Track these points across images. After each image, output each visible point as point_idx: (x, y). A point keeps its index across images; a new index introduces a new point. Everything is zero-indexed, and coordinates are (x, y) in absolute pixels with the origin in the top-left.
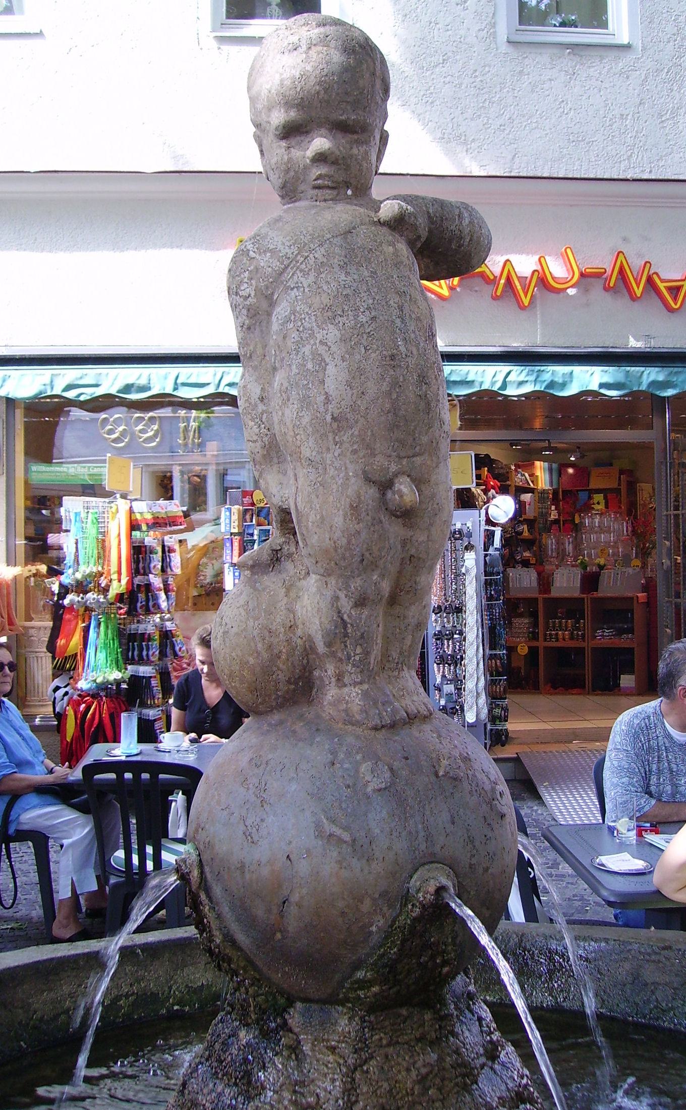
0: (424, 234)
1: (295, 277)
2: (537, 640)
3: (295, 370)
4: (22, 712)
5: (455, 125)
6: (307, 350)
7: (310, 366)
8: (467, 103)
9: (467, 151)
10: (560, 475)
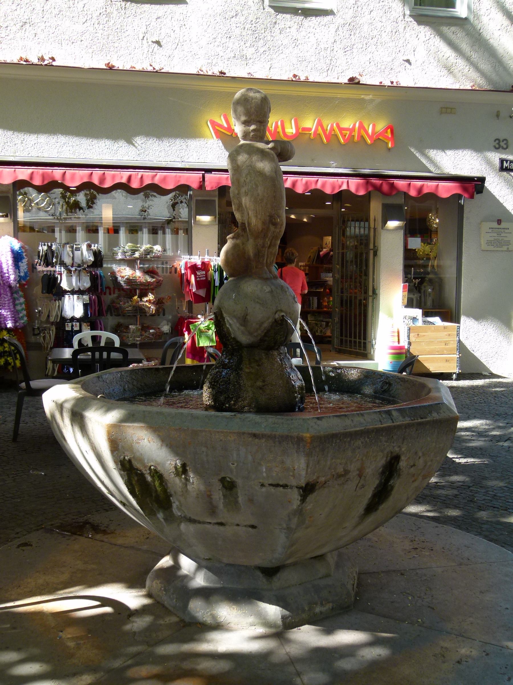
0: (279, 151)
4: (52, 294)
5: (241, 50)
7: (254, 186)
8: (247, 38)
9: (247, 64)
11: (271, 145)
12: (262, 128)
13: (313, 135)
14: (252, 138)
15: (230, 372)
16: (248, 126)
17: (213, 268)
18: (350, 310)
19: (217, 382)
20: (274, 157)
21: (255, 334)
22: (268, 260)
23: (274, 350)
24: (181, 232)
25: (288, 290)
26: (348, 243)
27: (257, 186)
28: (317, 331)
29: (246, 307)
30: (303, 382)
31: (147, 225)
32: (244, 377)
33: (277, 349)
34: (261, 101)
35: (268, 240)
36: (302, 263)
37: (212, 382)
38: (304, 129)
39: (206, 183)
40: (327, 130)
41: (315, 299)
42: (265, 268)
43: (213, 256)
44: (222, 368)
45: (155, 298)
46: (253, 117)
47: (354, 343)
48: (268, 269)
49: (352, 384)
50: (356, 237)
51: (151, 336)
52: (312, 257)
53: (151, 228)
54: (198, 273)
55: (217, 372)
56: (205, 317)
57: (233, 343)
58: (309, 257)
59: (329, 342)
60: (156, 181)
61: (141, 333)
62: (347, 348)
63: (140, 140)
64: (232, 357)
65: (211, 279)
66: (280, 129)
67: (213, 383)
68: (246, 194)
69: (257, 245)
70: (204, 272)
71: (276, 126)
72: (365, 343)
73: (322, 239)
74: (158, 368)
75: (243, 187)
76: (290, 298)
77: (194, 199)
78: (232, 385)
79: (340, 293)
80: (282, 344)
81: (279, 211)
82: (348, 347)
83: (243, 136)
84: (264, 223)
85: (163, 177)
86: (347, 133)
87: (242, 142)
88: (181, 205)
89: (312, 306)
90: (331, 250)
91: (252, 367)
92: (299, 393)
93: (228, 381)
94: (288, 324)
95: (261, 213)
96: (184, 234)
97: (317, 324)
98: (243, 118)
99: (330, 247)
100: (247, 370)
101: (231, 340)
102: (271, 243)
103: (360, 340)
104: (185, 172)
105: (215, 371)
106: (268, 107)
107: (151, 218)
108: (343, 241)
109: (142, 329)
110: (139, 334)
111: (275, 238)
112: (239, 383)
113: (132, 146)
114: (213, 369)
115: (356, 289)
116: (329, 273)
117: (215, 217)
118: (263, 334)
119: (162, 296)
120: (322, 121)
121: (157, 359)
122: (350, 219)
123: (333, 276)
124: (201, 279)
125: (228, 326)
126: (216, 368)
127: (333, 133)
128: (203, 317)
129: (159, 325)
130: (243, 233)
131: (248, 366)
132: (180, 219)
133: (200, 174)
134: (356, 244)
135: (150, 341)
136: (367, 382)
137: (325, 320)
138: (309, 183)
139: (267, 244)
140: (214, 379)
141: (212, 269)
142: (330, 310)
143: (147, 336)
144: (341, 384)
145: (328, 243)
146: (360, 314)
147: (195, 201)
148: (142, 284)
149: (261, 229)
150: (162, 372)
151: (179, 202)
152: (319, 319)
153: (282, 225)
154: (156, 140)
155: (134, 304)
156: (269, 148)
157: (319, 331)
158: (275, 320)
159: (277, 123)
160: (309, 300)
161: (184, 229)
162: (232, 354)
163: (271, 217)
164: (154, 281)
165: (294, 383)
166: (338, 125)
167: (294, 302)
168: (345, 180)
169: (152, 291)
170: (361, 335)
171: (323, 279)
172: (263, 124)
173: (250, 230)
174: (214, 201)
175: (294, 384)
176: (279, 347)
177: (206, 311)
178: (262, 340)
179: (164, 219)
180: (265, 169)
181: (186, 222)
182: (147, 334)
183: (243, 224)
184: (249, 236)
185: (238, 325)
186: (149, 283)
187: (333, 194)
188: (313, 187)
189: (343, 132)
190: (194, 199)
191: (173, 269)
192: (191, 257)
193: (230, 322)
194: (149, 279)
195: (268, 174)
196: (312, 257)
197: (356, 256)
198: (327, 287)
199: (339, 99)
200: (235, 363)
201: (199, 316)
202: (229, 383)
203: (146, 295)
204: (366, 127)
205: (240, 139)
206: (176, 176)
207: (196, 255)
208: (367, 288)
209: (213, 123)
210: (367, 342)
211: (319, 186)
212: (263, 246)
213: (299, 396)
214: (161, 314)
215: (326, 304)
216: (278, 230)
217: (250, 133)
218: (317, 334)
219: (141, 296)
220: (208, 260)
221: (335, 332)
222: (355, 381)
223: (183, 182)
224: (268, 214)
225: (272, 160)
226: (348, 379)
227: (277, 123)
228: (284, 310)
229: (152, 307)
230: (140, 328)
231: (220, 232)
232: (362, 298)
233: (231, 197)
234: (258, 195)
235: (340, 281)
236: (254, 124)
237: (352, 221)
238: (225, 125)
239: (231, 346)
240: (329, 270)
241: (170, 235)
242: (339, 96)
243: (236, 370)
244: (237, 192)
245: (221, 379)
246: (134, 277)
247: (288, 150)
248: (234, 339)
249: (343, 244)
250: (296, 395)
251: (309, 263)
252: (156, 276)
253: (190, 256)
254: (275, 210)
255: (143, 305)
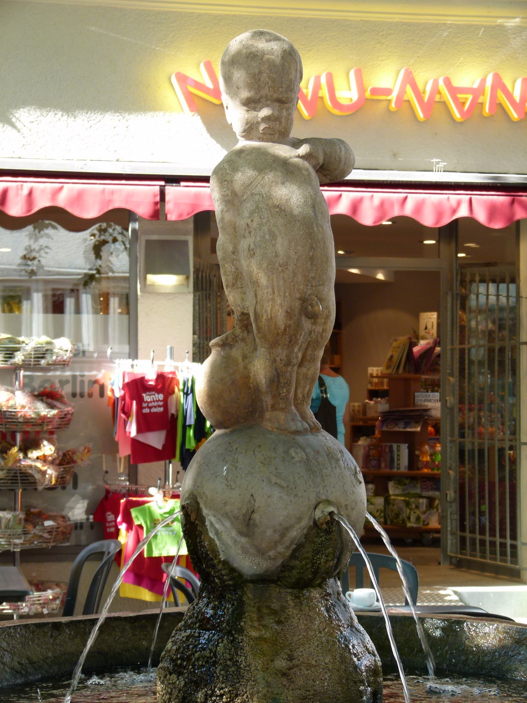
0: (321, 161)
1: (258, 188)
2: (480, 540)
3: (258, 239)
6: (265, 228)
7: (267, 237)
10: (14, 463)
11: (304, 149)
12: (285, 113)
13: (396, 103)
14: (264, 134)
15: (216, 637)
16: (254, 109)
17: (181, 387)
18: (479, 471)
19: (189, 659)
20: (309, 175)
21: (272, 553)
22: (299, 391)
23: (314, 587)
24: (114, 303)
25: (343, 456)
26: (473, 323)
27: (273, 236)
28: (409, 518)
29: (252, 495)
30: (378, 658)
31: (41, 286)
32: (247, 648)
33: (320, 586)
34: (283, 58)
35: (299, 350)
36: (375, 369)
37: (177, 659)
38: (374, 91)
39: (169, 206)
40: (424, 92)
41: (404, 450)
42: (293, 408)
43: (183, 360)
44: (200, 627)
45: (57, 450)
46: (265, 91)
47: (490, 546)
48: (298, 411)
49: (486, 659)
50: (489, 310)
51: (46, 535)
52: (395, 359)
53: (50, 293)
54: (147, 397)
55: (188, 637)
56: (164, 492)
57: (223, 572)
58: (388, 356)
59: (436, 543)
60: (61, 201)
61: (24, 527)
62: (475, 556)
63: (26, 114)
64: (220, 603)
65: (177, 411)
66: (324, 92)
67: (179, 662)
68: (251, 253)
69: (275, 361)
70: (161, 397)
71: (317, 87)
72: (514, 547)
73: (417, 318)
74: (60, 623)
75: (244, 237)
76: (347, 473)
77: (143, 239)
78: (220, 667)
79: (456, 437)
80: (329, 574)
81: (321, 288)
82: (478, 554)
83: (244, 131)
84: (289, 314)
85: (75, 193)
86: (466, 99)
87: (242, 143)
88: (113, 246)
89: (398, 464)
90: (437, 343)
91: (264, 626)
92: (368, 682)
93: (211, 658)
94: (344, 531)
95: (282, 294)
96: (119, 311)
97: (408, 504)
98: (245, 94)
99: (435, 335)
100: (254, 634)
101: (220, 567)
102: (304, 357)
103: (503, 540)
104: (123, 182)
105: (184, 634)
106: (296, 70)
107: (49, 271)
108: (462, 320)
109: (26, 520)
110: (19, 530)
111: (311, 344)
112: (236, 663)
113: (10, 128)
114: (180, 630)
115: (492, 426)
116: (433, 391)
117: (188, 278)
118: (288, 553)
119: (70, 445)
120: (414, 74)
121: (58, 585)
122: (477, 278)
123: (443, 400)
124: (154, 410)
125: (212, 535)
126: (187, 626)
127: (437, 98)
128: (161, 492)
129: (63, 509)
130: (245, 334)
131: (256, 624)
132: (110, 274)
133: (154, 187)
134: (490, 326)
135: (44, 545)
136: (520, 654)
137: (425, 494)
138: (387, 206)
139: (297, 357)
140: (182, 653)
141: (179, 389)
142: (435, 471)
143: (37, 536)
144: (463, 658)
145: (429, 326)
146: (502, 480)
147: (143, 244)
148: (27, 421)
149: (282, 327)
150: (67, 631)
151: (110, 239)
152: (413, 491)
153: (328, 317)
154: (62, 116)
155: (10, 464)
156: (299, 156)
157: (413, 519)
158: (315, 523)
159: (318, 79)
160: (391, 451)
161: (121, 296)
162: (221, 597)
163: (304, 300)
164: (54, 415)
165: (359, 660)
166: (448, 82)
167: (355, 481)
168: (464, 197)
169: (50, 435)
170: (505, 499)
171: (421, 405)
172: (287, 105)
173: (259, 329)
174: (186, 243)
175: (357, 662)
176: (324, 580)
177: (166, 478)
178: (285, 567)
179: (79, 274)
180: (292, 201)
181: (125, 279)
182: (36, 531)
183: (245, 316)
184: (257, 340)
185: (234, 533)
186: (43, 420)
187: (438, 226)
188: (396, 212)
189: (459, 96)
190: (143, 239)
191: (96, 389)
192: (136, 362)
193: (217, 526)
194: (44, 410)
195: (296, 211)
196: (395, 359)
197: (491, 351)
198: (430, 422)
199: (449, 28)
200: (227, 618)
201: (152, 490)
202: (215, 663)
203: (36, 445)
204: (508, 85)
205: (239, 137)
206: (103, 191)
207: (147, 357)
208: (515, 426)
209: (182, 79)
210: (519, 544)
211: (408, 211)
212: (288, 363)
213: (369, 689)
214: (70, 486)
215: (428, 459)
216: (319, 329)
217: (258, 123)
218: (409, 525)
219: (25, 449)
220: (172, 370)
221: (449, 521)
222: (492, 652)
223: (117, 204)
224: (298, 295)
225: (304, 181)
226: (477, 646)
227: (318, 79)
228: (332, 498)
229: (50, 472)
230: (22, 516)
231: (197, 308)
232: (507, 445)
233: (219, 258)
234: (276, 256)
235: (456, 410)
236: (267, 106)
237: (482, 281)
238: (210, 85)
239: (219, 578)
240: (434, 386)
241: (91, 316)
242: (449, 21)
243: (229, 633)
244: (231, 248)
245: (196, 652)
246: (11, 407)
247: (340, 161)
248: (226, 563)
249: (462, 328)
250: (362, 688)
251: (389, 371)
252: (58, 404)
253: (133, 360)
254: (312, 286)
255: (31, 467)
